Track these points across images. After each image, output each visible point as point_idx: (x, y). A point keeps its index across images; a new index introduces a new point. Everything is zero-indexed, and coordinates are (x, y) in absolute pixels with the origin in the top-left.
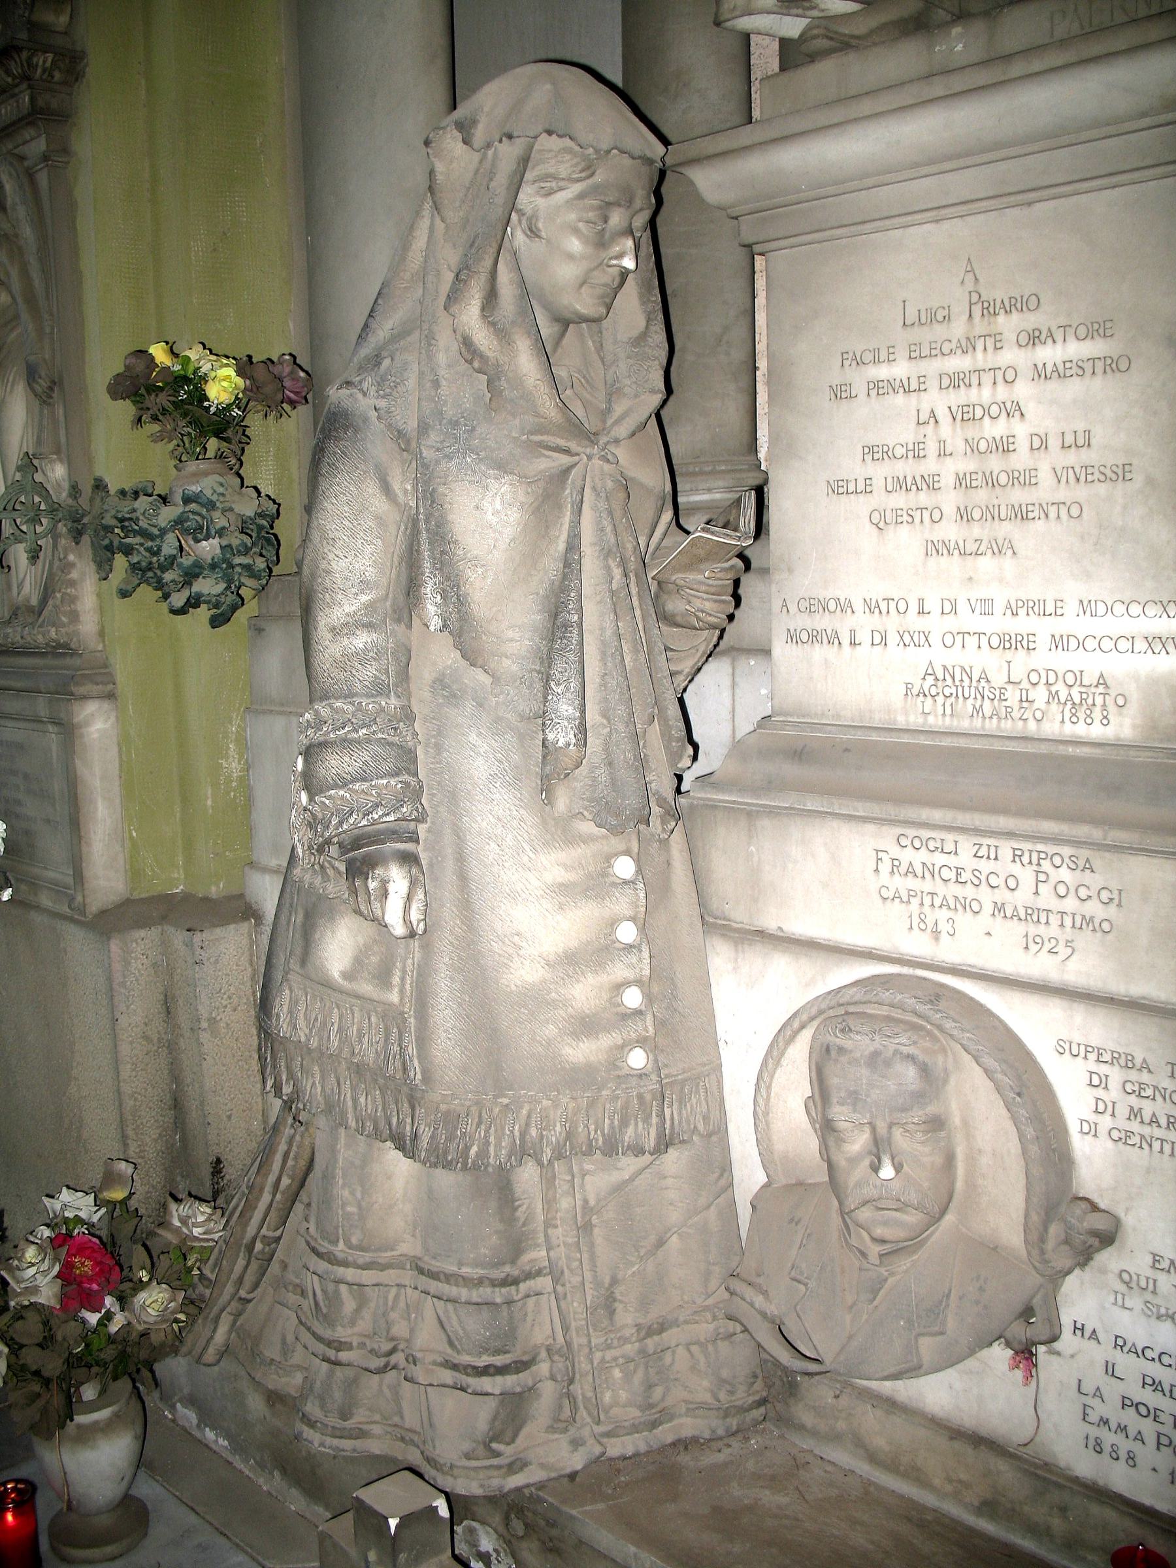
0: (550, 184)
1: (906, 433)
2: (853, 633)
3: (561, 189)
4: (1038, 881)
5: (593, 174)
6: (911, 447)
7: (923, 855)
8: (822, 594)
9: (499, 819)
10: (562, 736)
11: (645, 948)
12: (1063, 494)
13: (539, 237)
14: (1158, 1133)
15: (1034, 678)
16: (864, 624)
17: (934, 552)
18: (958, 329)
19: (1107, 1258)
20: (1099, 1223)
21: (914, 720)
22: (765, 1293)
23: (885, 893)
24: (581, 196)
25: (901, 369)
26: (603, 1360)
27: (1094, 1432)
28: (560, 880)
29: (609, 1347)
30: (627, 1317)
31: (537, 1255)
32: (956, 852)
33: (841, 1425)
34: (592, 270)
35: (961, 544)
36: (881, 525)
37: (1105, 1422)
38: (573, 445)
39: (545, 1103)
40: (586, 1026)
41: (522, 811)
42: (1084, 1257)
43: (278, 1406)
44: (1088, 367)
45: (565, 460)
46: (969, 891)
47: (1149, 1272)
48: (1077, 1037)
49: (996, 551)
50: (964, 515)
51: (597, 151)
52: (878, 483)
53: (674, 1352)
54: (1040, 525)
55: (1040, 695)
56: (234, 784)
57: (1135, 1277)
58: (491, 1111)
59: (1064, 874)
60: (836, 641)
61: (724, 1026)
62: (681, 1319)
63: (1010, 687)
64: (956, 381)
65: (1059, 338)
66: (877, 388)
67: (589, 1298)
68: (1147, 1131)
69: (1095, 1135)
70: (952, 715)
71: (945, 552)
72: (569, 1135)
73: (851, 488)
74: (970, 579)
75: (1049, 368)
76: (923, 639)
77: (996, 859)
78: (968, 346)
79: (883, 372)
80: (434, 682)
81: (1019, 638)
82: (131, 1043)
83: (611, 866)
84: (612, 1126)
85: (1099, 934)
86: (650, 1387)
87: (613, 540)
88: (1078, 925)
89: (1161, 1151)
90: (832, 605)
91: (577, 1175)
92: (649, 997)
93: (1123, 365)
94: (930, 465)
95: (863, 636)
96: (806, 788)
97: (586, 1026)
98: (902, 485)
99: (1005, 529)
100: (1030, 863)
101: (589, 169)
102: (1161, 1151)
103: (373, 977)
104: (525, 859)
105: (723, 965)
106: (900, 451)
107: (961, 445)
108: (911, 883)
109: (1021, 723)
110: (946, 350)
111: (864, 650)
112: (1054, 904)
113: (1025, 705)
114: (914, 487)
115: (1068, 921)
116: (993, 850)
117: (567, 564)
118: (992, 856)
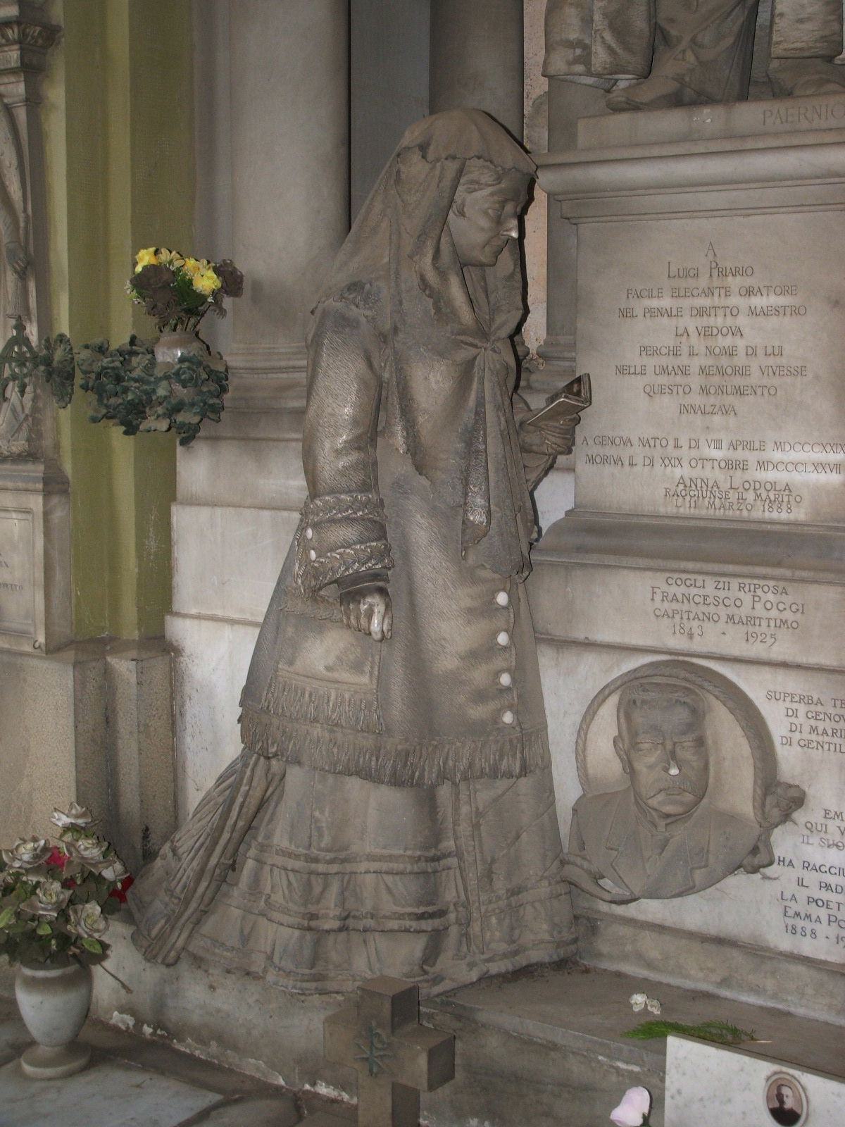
0: (475, 185)
1: (668, 341)
2: (631, 458)
3: (481, 189)
4: (754, 601)
5: (500, 183)
6: (671, 348)
7: (683, 589)
8: (611, 434)
9: (434, 568)
10: (477, 517)
11: (513, 649)
12: (765, 381)
13: (464, 216)
14: (826, 739)
15: (747, 486)
16: (638, 452)
17: (685, 412)
18: (703, 282)
19: (799, 816)
20: (793, 793)
21: (671, 510)
22: (589, 861)
23: (657, 612)
24: (492, 194)
25: (666, 302)
26: (487, 911)
27: (790, 922)
28: (468, 605)
29: (490, 902)
30: (500, 885)
31: (449, 844)
32: (704, 587)
33: (629, 948)
34: (492, 238)
35: (702, 407)
36: (651, 394)
37: (797, 914)
38: (476, 342)
39: (459, 744)
40: (480, 696)
41: (448, 563)
42: (786, 817)
44: (782, 311)
45: (473, 351)
46: (712, 609)
47: (823, 821)
48: (779, 689)
49: (724, 412)
50: (705, 390)
51: (503, 169)
52: (650, 370)
53: (525, 908)
54: (752, 398)
55: (750, 496)
56: (152, 557)
57: (814, 825)
58: (427, 749)
59: (770, 596)
60: (620, 463)
61: (550, 703)
62: (529, 886)
63: (731, 491)
64: (701, 312)
65: (765, 292)
66: (650, 312)
67: (479, 870)
68: (820, 739)
69: (790, 745)
70: (695, 507)
71: (692, 412)
72: (471, 765)
73: (632, 370)
74: (708, 428)
75: (758, 310)
76: (677, 462)
77: (729, 589)
78: (709, 292)
79: (655, 303)
80: (393, 484)
81: (738, 463)
82: (84, 744)
83: (494, 598)
84: (495, 760)
85: (791, 630)
86: (512, 929)
87: (500, 401)
88: (778, 625)
89: (829, 750)
90: (618, 441)
91: (472, 791)
92: (513, 679)
93: (802, 311)
94: (684, 360)
95: (639, 460)
96: (601, 551)
97: (480, 696)
98: (665, 370)
99: (729, 400)
100: (750, 591)
101: (499, 179)
102: (829, 750)
103: (351, 668)
104: (449, 593)
105: (547, 661)
106: (664, 351)
107: (703, 350)
108: (675, 606)
109: (738, 512)
110: (695, 293)
111: (639, 468)
112: (764, 614)
113: (741, 501)
114: (673, 373)
115: (772, 624)
116: (727, 584)
117: (477, 413)
118: (726, 588)
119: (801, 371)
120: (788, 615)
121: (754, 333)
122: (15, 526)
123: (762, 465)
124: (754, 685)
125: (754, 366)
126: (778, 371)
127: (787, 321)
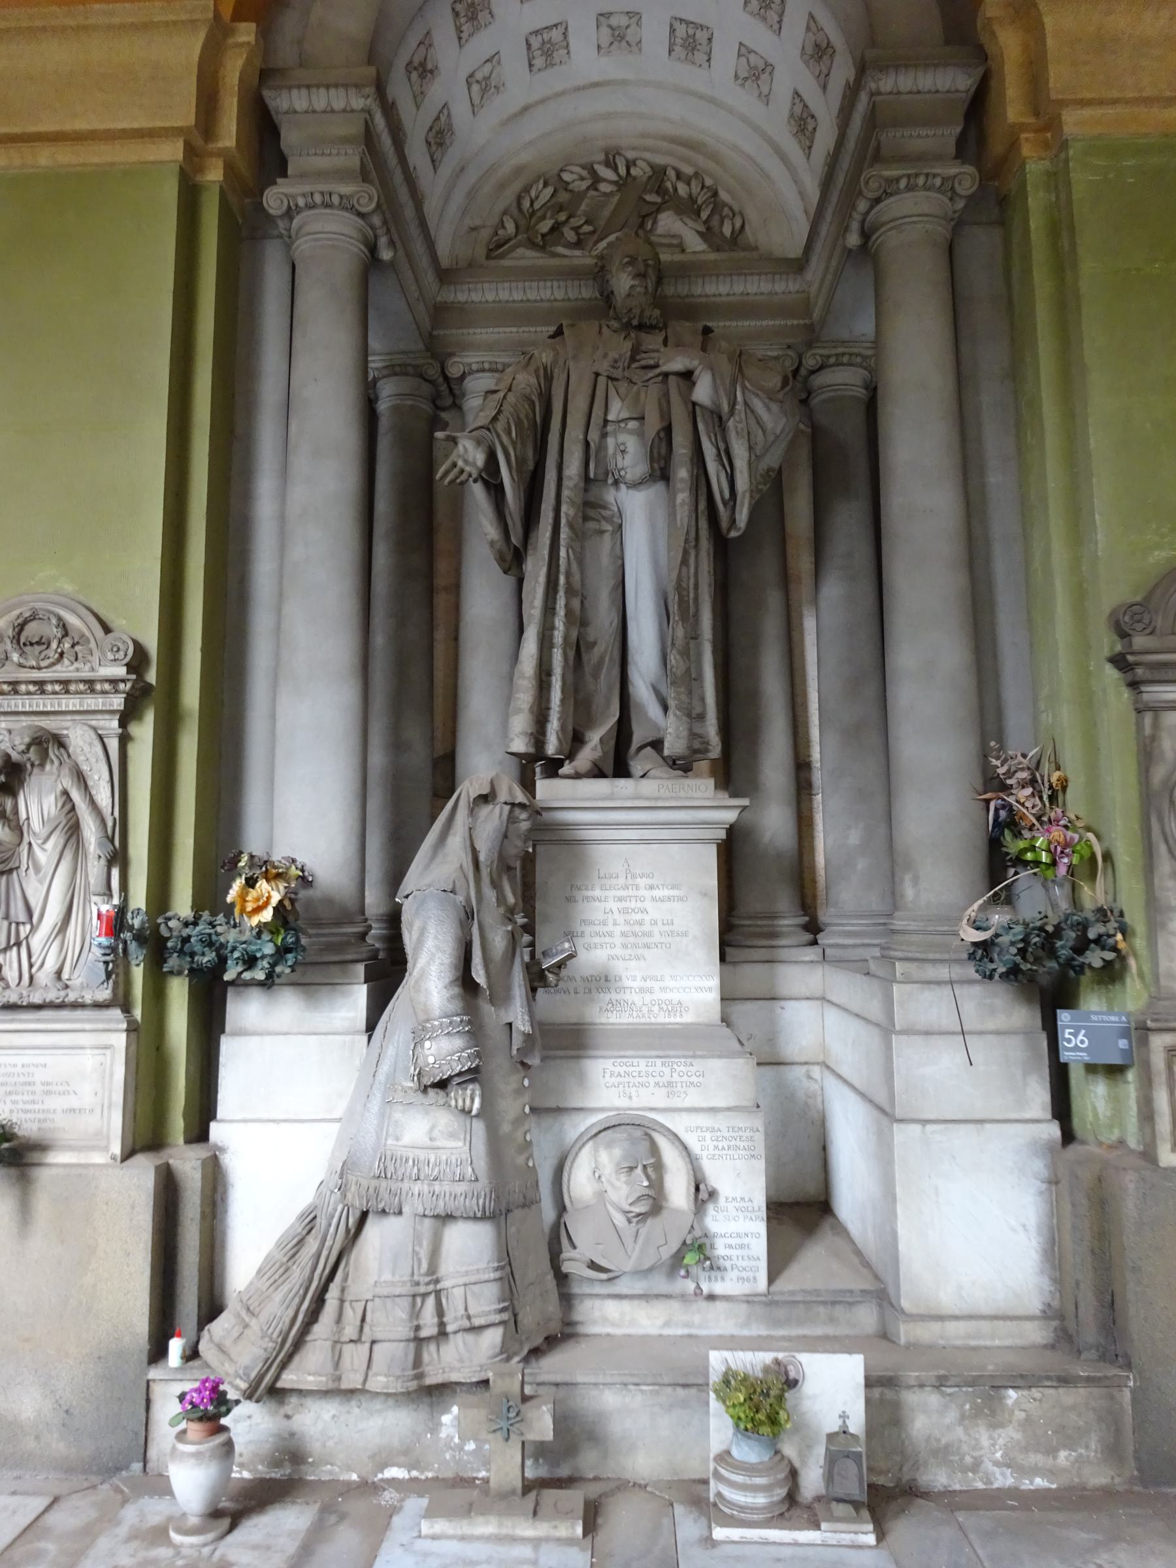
2: (576, 989)
7: (625, 1068)
12: (663, 940)
43: (225, 1449)
46: (644, 1079)
50: (624, 946)
54: (655, 950)
59: (682, 1068)
64: (620, 899)
99: (640, 951)
108: (619, 1079)
119: (685, 934)
120: (694, 1079)
121: (655, 912)
122: (88, 1061)
123: (663, 989)
124: (677, 1124)
125: (656, 930)
126: (671, 934)
127: (677, 906)
